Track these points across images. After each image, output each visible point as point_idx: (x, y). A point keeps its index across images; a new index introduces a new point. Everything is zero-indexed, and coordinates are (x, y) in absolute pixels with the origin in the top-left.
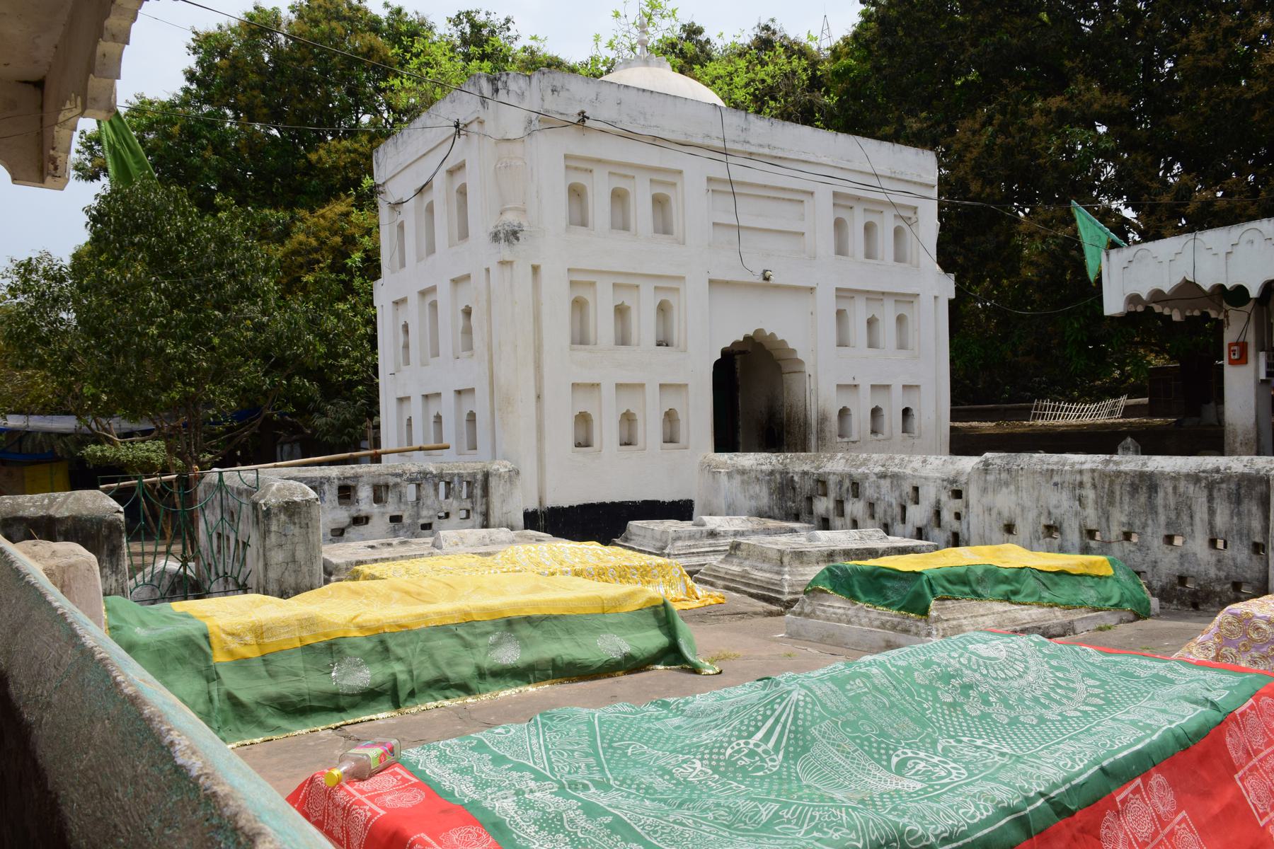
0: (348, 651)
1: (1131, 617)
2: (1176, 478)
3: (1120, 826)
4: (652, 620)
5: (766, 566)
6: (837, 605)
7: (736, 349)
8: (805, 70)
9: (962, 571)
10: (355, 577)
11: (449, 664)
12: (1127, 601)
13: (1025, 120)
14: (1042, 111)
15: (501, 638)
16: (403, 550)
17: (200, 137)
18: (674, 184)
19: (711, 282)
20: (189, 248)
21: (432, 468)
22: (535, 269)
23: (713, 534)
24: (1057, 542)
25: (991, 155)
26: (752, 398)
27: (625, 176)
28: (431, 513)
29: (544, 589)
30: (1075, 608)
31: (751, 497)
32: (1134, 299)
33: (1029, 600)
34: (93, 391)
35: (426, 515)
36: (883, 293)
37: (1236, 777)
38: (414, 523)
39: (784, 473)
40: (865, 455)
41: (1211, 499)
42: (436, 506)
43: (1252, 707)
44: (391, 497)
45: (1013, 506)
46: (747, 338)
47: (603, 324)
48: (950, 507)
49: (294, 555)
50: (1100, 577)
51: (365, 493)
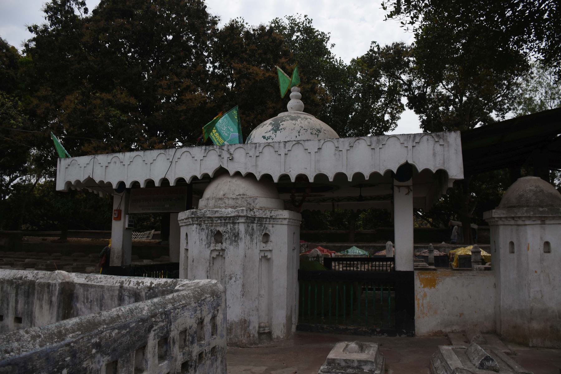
32: (69, 184)
41: (17, 295)
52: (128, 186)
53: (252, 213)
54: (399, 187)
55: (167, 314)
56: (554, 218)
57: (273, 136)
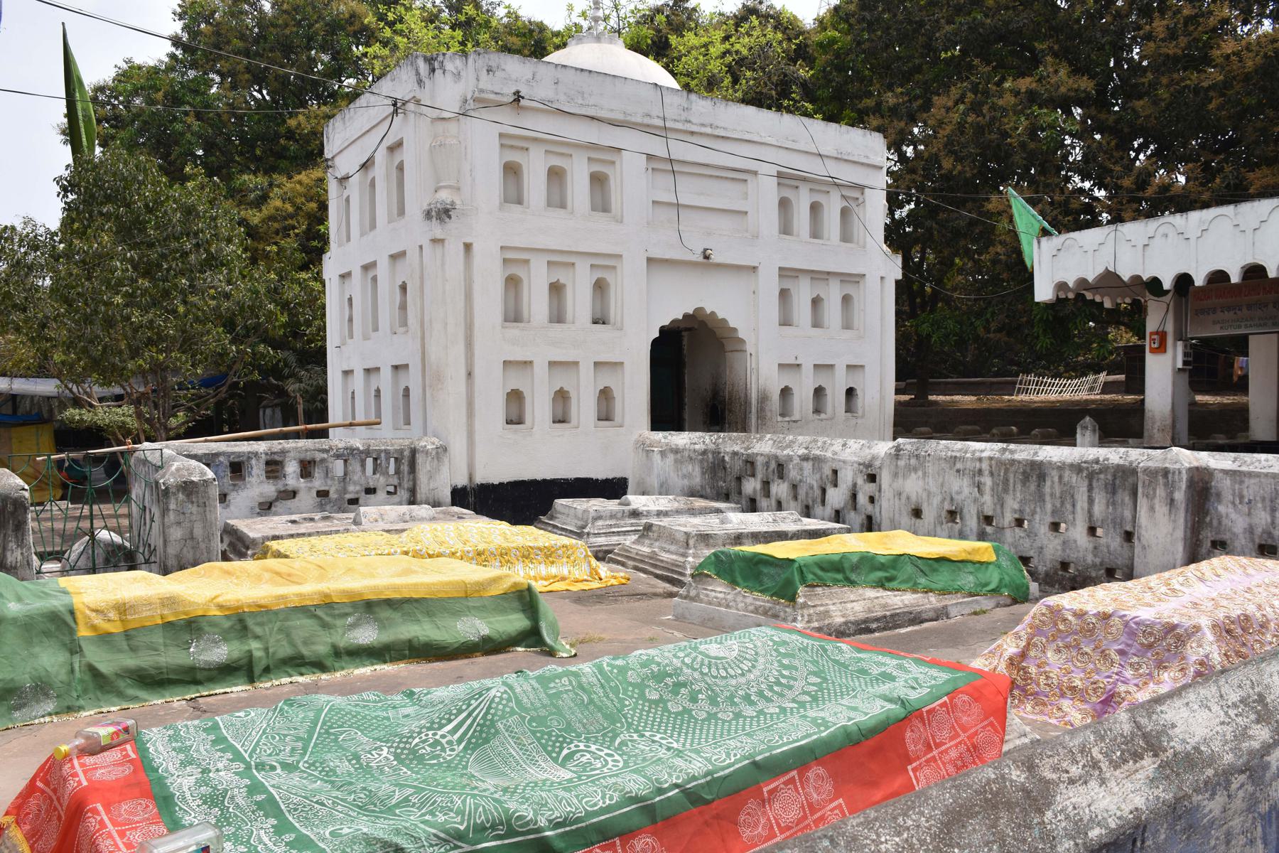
0: (207, 629)
1: (1009, 601)
2: (1061, 467)
3: (765, 813)
4: (516, 604)
5: (673, 548)
6: (719, 589)
7: (682, 326)
8: (780, 43)
9: (837, 558)
10: (264, 554)
11: (305, 643)
12: (1006, 586)
13: (995, 99)
14: (1011, 91)
15: (359, 619)
16: (322, 526)
17: (184, 103)
18: (613, 163)
19: (649, 260)
20: (157, 217)
21: (358, 444)
22: (468, 247)
23: (635, 514)
24: (957, 527)
25: (962, 133)
26: (690, 376)
27: (562, 154)
28: (358, 488)
29: (415, 572)
30: (950, 593)
31: (684, 476)
32: (1062, 286)
33: (903, 587)
34: (63, 357)
35: (353, 490)
36: (828, 273)
37: (909, 767)
38: (341, 498)
39: (716, 453)
40: (791, 437)
41: (1090, 488)
42: (363, 481)
43: (944, 705)
44: (318, 473)
45: (920, 491)
46: (686, 316)
47: (537, 302)
48: (865, 489)
49: (191, 533)
50: (981, 563)
51: (292, 468)
52: (1199, 281)
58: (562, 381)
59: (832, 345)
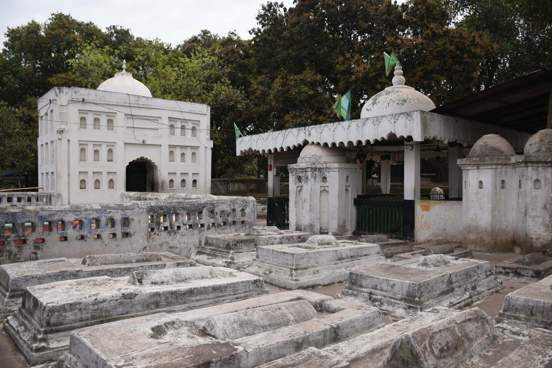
19: (125, 143)
26: (140, 175)
51: (15, 199)
53: (314, 166)
54: (407, 145)
55: (213, 204)
56: (484, 165)
57: (372, 108)
58: (97, 177)
59: (189, 167)
